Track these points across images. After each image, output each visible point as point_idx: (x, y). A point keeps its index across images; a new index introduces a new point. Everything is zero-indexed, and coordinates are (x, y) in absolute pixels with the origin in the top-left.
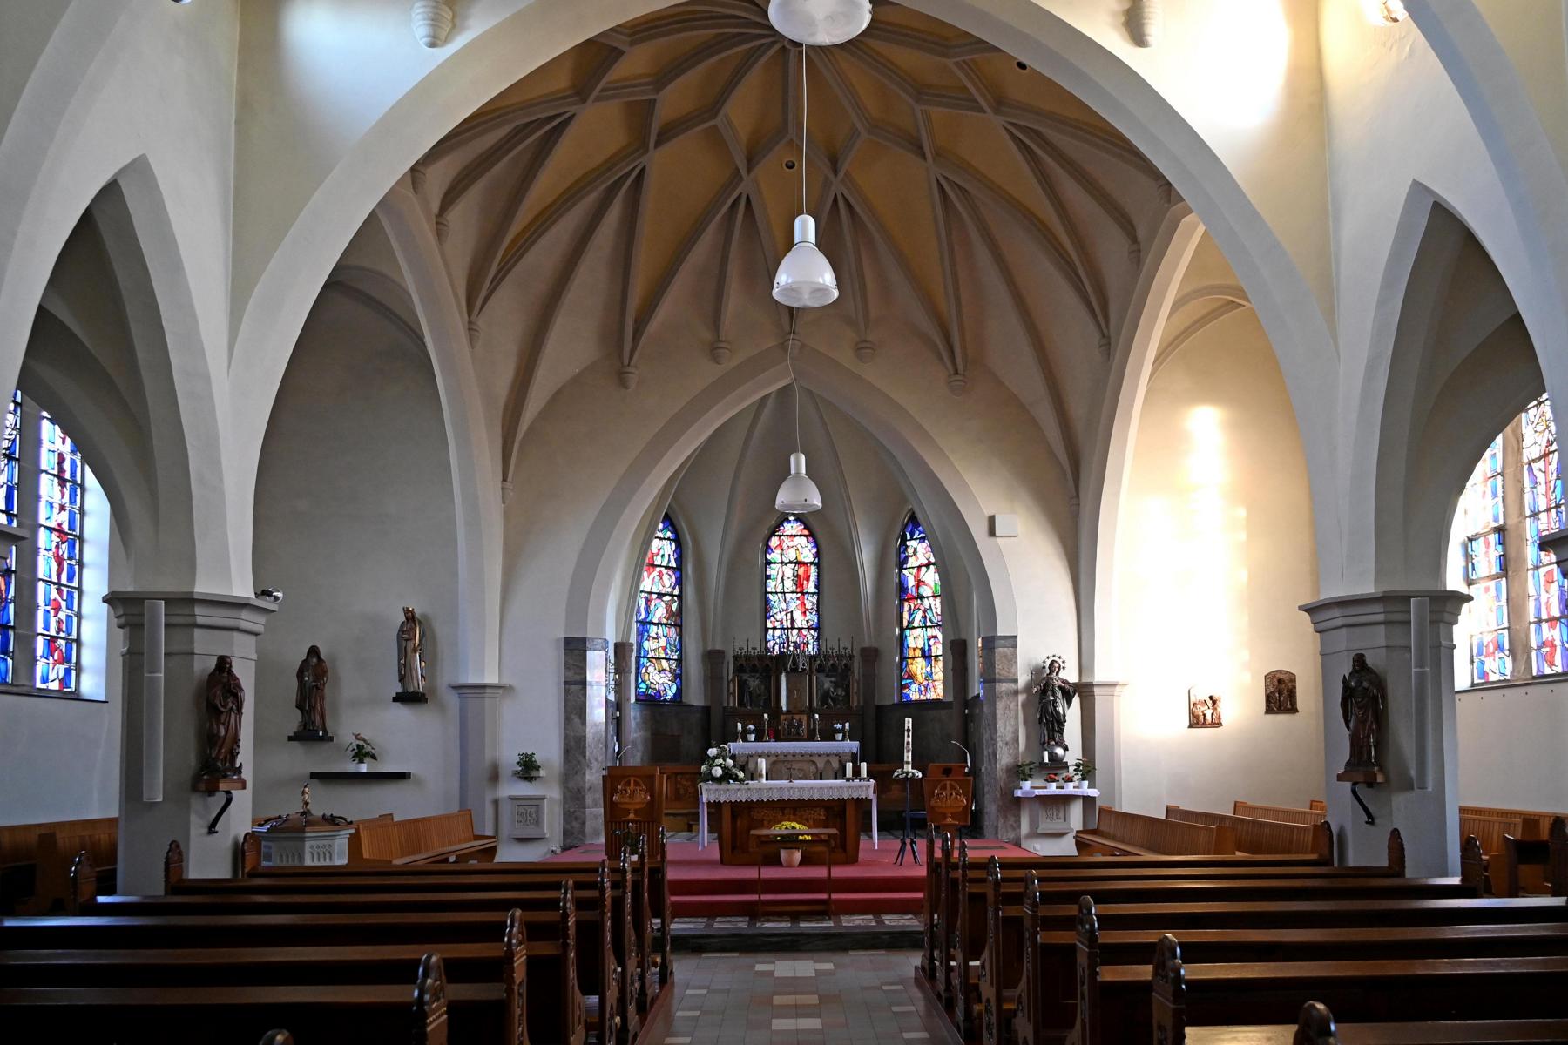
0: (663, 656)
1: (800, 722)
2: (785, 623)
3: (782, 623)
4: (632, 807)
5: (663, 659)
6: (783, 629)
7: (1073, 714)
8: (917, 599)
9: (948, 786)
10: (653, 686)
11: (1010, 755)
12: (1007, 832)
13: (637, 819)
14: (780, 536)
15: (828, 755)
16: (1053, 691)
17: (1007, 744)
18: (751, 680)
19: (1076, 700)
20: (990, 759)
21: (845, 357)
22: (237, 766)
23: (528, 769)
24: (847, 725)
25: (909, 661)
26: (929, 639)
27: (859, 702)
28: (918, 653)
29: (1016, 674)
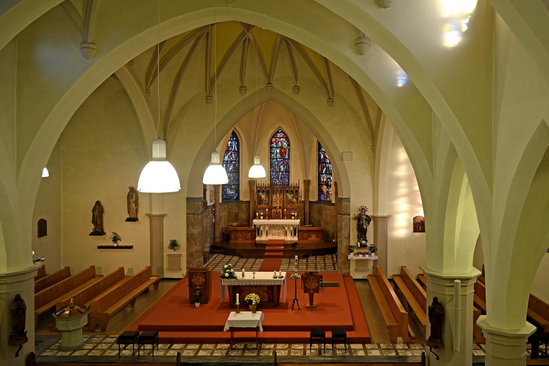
0: (232, 184)
1: (280, 211)
2: (277, 170)
3: (276, 170)
4: (198, 284)
5: (232, 185)
6: (276, 172)
7: (370, 229)
8: (324, 163)
9: (311, 279)
10: (228, 195)
11: (347, 242)
12: (345, 270)
13: (200, 288)
14: (275, 138)
16: (362, 219)
17: (346, 238)
18: (263, 195)
19: (372, 222)
20: (339, 243)
21: (289, 92)
22: (25, 332)
23: (174, 245)
24: (296, 214)
25: (321, 186)
26: (328, 179)
28: (324, 183)
29: (350, 212)
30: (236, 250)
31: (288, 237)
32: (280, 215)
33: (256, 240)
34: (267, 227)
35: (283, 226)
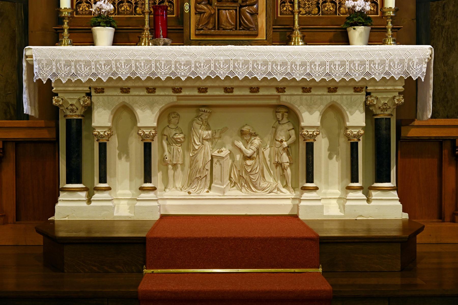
15: (125, 90)
30: (284, 172)
31: (323, 190)
32: (254, 14)
33: (57, 217)
34: (151, 106)
35: (285, 99)
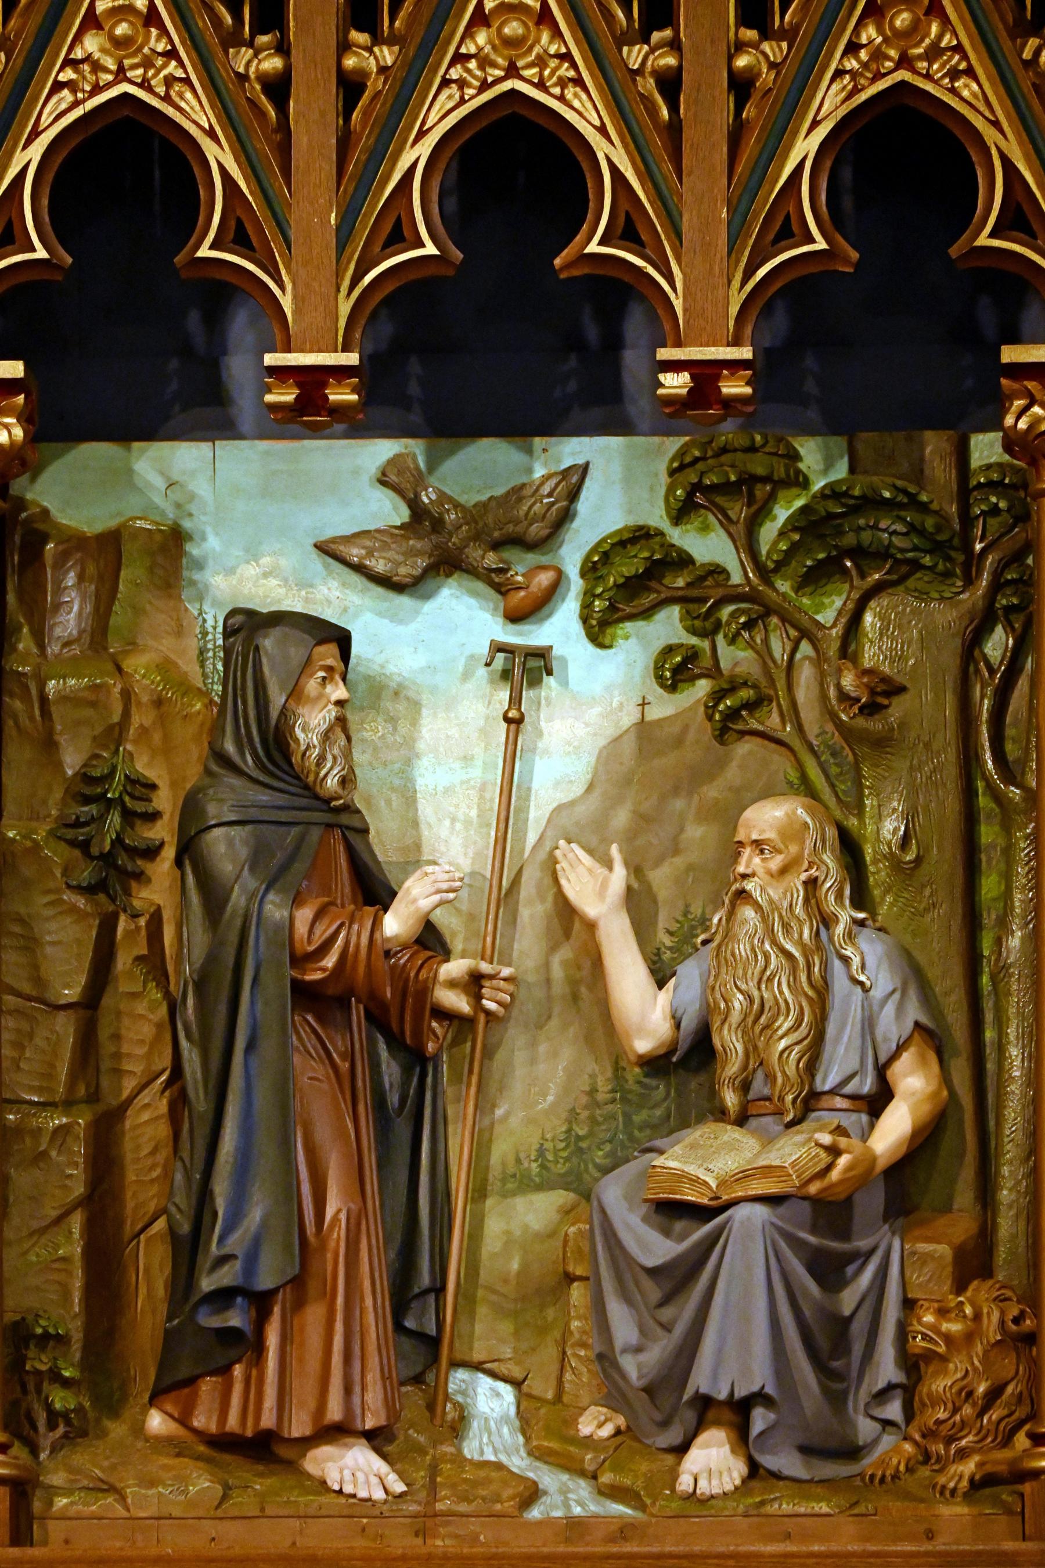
27: (245, 52)
